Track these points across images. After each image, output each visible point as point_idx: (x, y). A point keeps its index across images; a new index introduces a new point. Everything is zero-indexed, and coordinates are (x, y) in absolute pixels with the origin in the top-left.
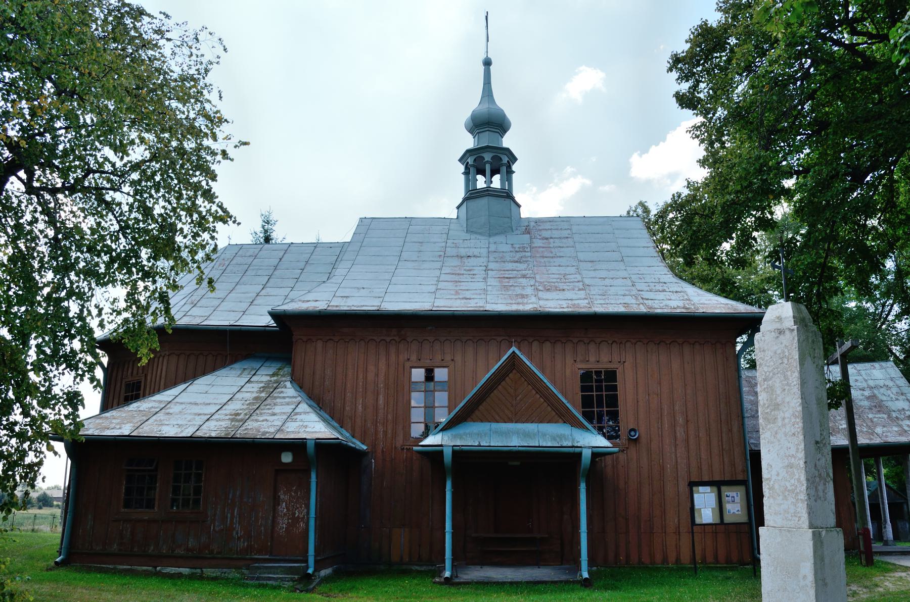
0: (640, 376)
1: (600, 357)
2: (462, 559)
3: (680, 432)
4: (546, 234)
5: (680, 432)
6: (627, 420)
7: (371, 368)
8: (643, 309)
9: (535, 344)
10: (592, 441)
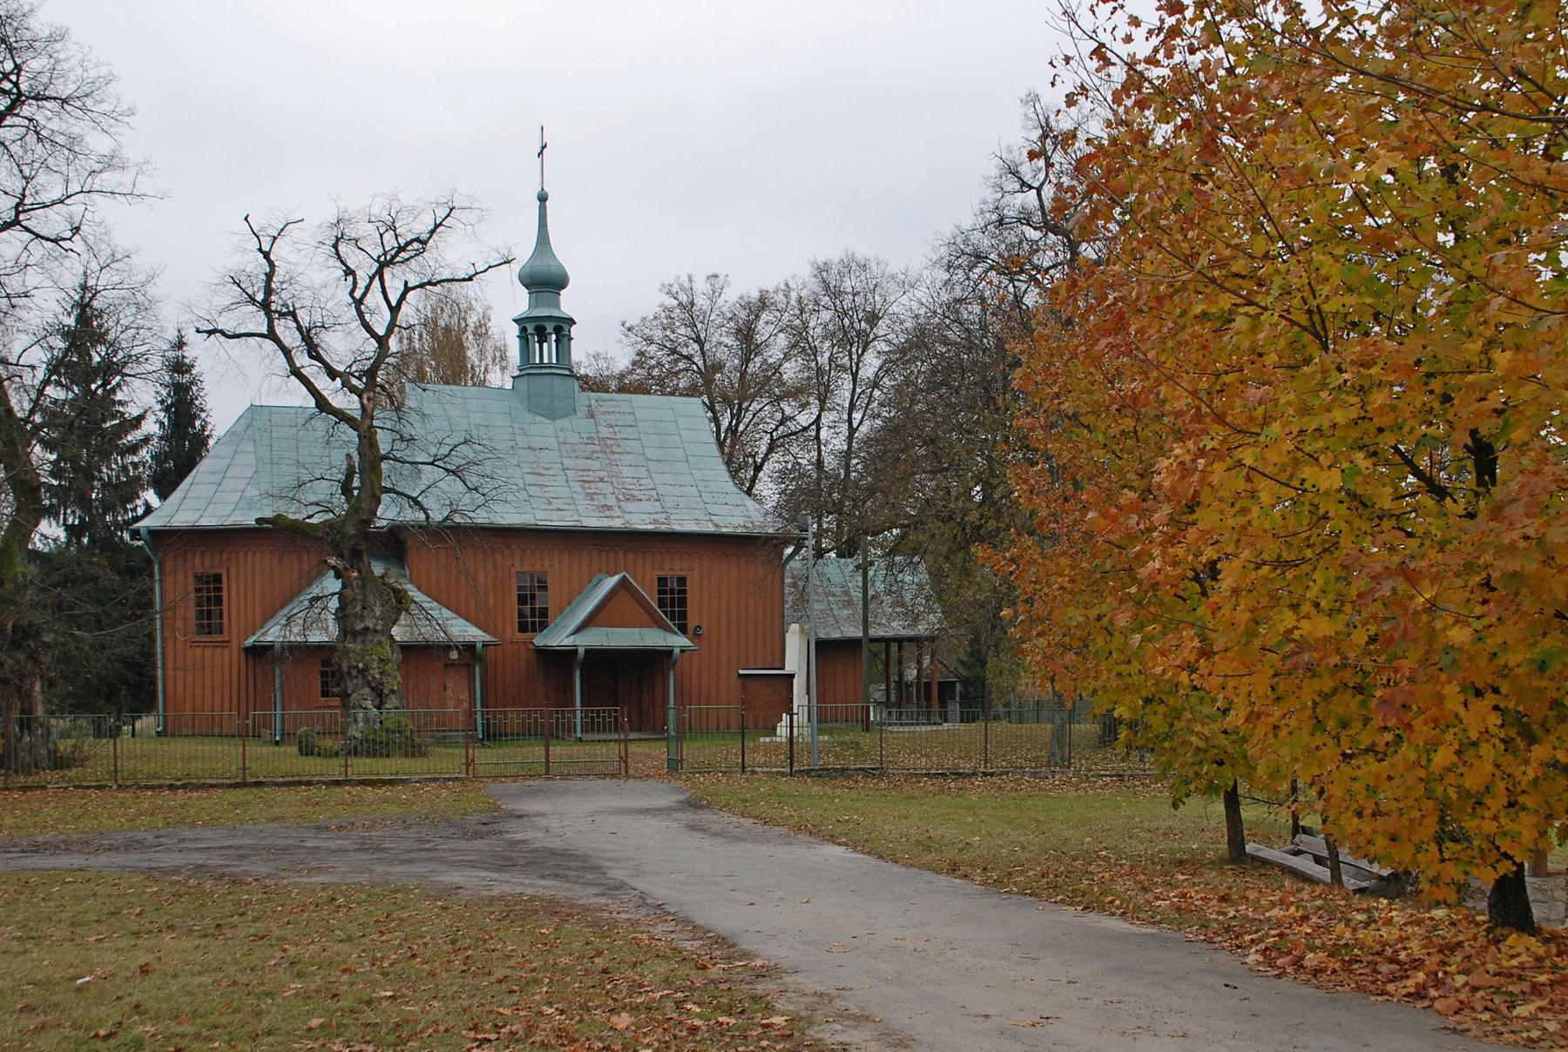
0: (706, 586)
1: (673, 567)
2: (585, 730)
3: (734, 630)
4: (611, 419)
5: (734, 630)
6: (692, 621)
7: (481, 573)
8: (711, 529)
9: (621, 554)
10: (679, 641)
